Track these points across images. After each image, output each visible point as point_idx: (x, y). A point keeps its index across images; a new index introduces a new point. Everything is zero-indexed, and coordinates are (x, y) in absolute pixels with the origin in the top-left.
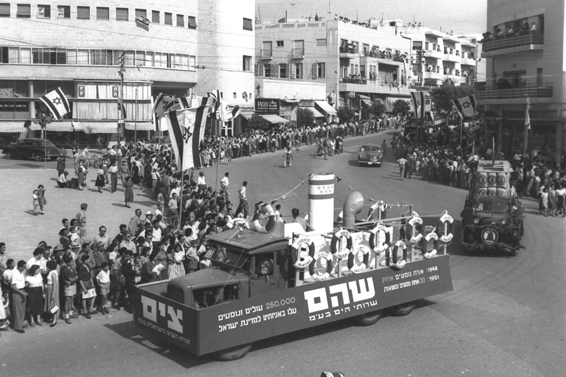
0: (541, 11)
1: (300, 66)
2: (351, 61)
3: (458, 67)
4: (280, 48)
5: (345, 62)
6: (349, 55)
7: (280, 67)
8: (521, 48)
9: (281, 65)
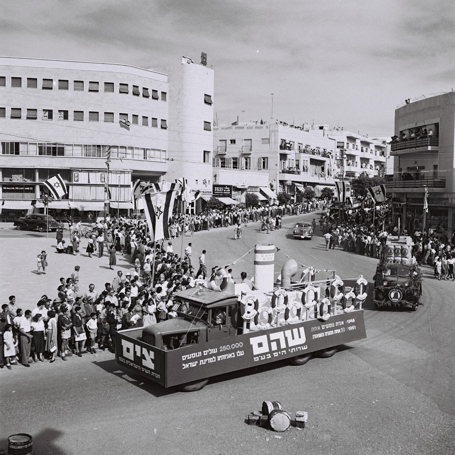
0: (437, 120)
1: (248, 159)
2: (288, 157)
3: (372, 162)
4: (233, 145)
5: (283, 157)
6: (286, 152)
7: (232, 160)
8: (421, 149)
9: (234, 159)
